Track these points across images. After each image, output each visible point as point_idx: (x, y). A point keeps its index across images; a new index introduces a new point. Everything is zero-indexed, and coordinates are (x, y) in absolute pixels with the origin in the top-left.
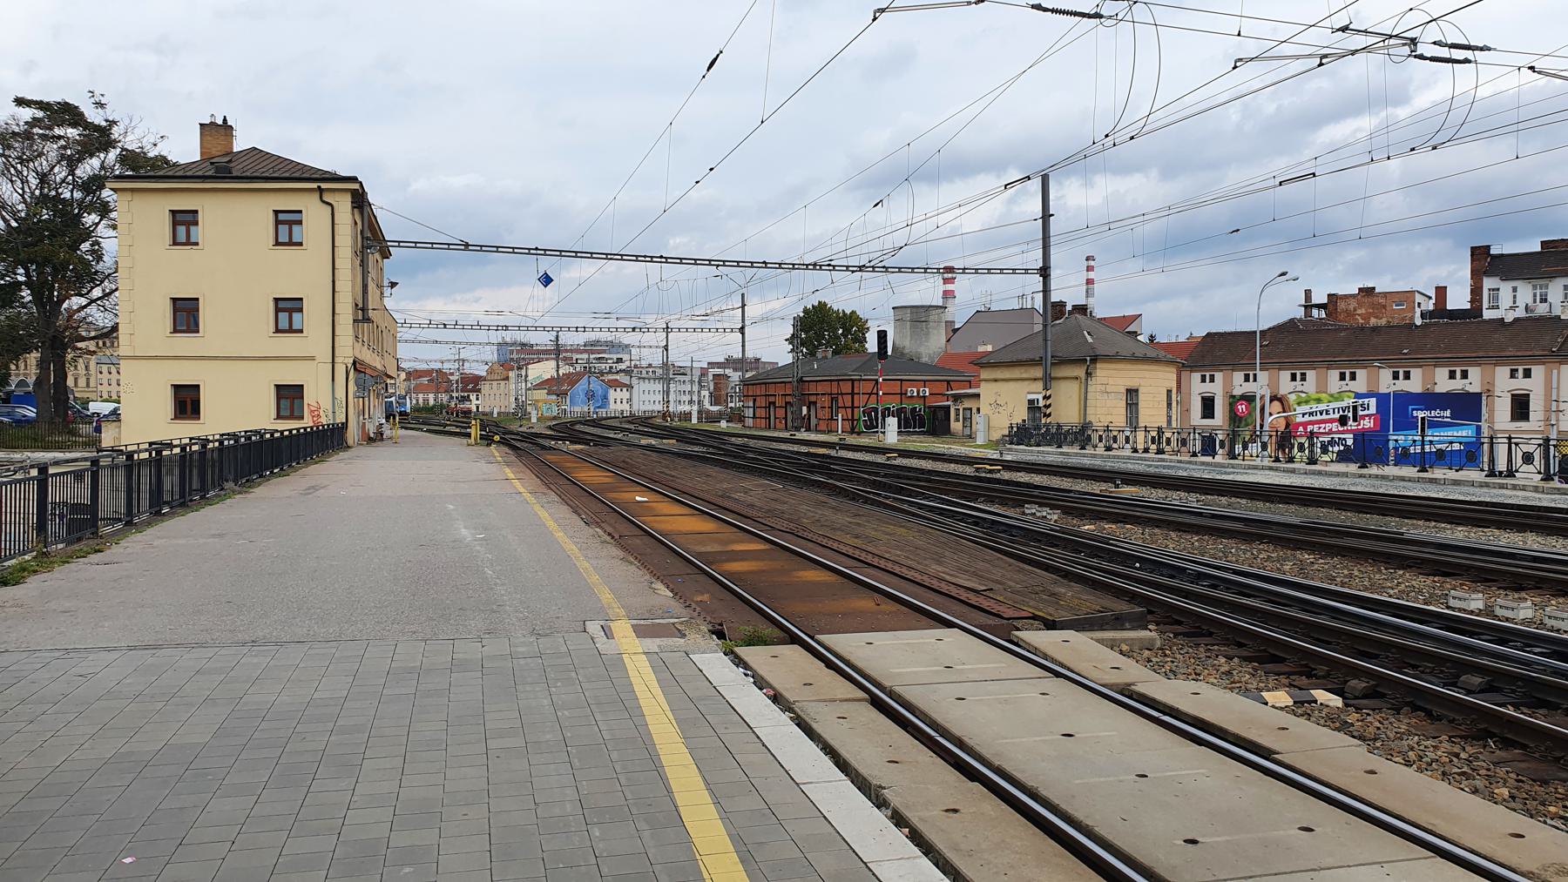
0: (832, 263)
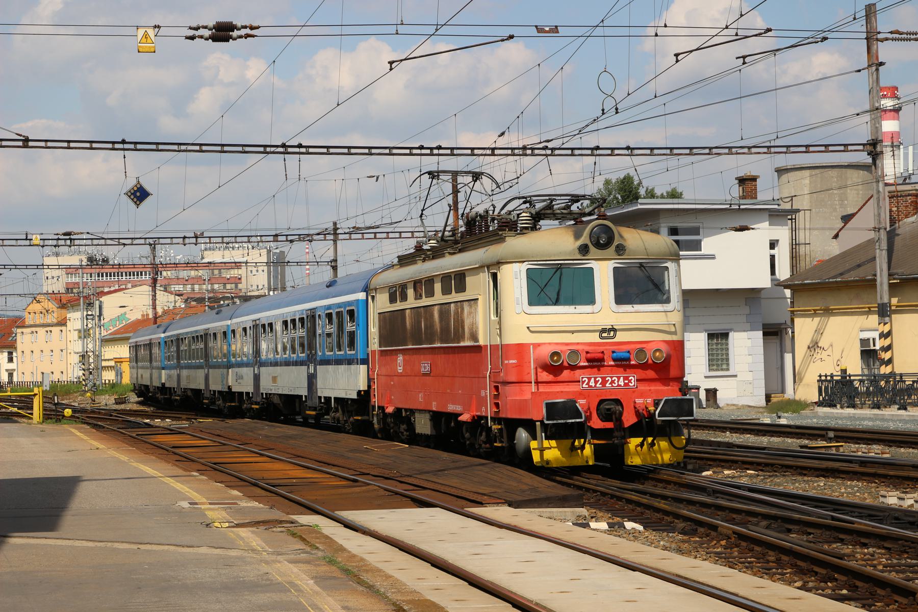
0: (550, 145)
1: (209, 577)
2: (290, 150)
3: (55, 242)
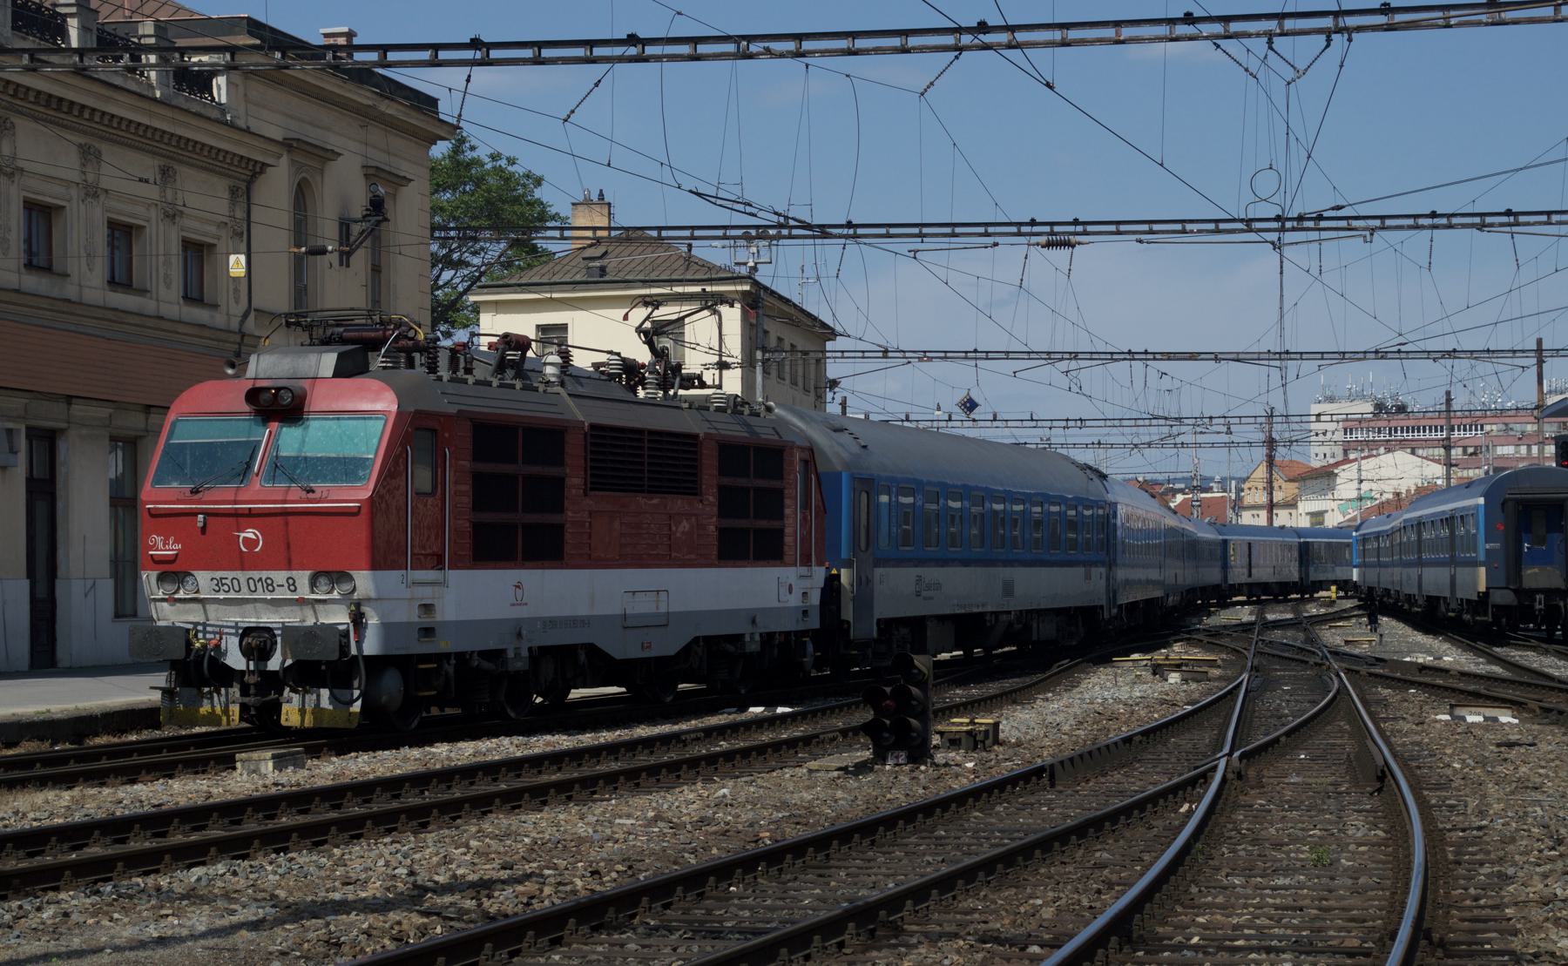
1: (1326, 919)
2: (1136, 356)
3: (1064, 424)
